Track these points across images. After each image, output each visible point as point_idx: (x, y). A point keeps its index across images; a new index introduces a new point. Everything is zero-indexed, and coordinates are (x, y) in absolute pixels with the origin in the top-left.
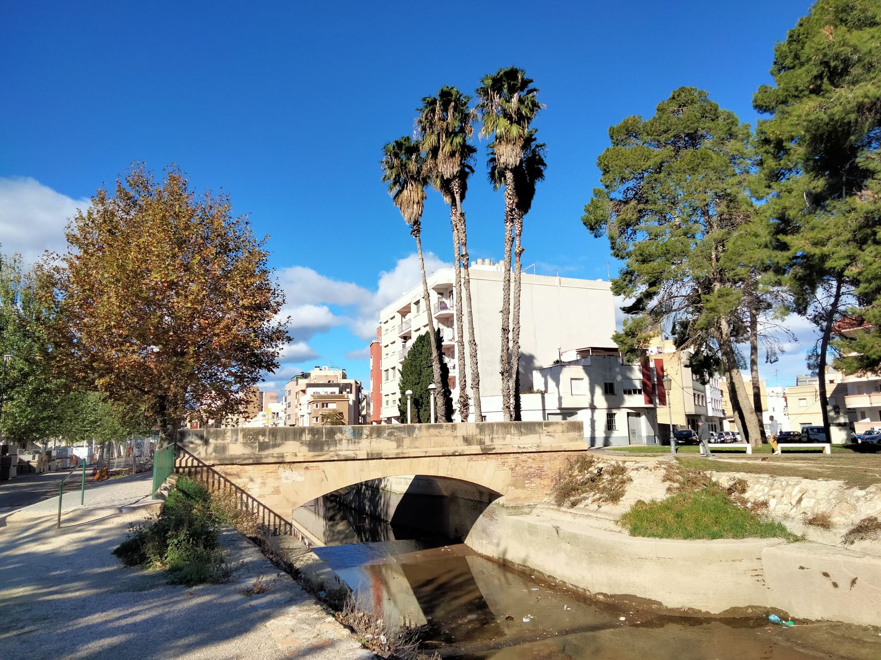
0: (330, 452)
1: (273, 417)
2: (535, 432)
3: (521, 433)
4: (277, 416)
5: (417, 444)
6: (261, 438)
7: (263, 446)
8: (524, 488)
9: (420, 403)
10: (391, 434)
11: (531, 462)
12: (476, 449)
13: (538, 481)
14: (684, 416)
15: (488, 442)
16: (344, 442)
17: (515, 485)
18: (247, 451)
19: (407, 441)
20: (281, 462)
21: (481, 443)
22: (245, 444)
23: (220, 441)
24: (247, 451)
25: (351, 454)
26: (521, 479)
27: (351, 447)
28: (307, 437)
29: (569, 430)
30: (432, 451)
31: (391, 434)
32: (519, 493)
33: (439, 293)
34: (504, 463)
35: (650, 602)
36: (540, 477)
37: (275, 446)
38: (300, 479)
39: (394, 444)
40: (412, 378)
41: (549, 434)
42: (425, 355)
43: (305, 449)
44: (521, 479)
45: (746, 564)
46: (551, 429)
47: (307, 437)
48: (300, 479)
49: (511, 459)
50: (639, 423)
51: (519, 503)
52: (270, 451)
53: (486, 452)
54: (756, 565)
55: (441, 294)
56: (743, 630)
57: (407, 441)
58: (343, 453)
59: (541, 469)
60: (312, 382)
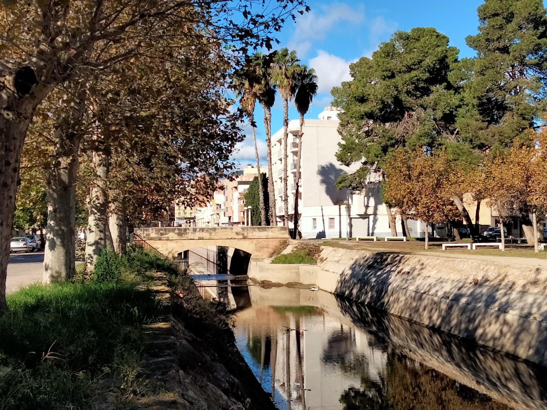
0: (185, 237)
1: (217, 208)
2: (266, 231)
3: (260, 231)
4: (220, 207)
5: (217, 234)
6: (161, 232)
7: (162, 234)
8: (260, 251)
9: (255, 212)
10: (207, 231)
11: (264, 243)
12: (241, 237)
13: (266, 249)
14: (490, 217)
15: (246, 234)
16: (190, 233)
17: (257, 250)
18: (157, 236)
19: (213, 233)
20: (168, 240)
21: (243, 234)
22: (156, 233)
23: (147, 232)
24: (157, 236)
25: (192, 238)
26: (260, 248)
27: (193, 235)
28: (177, 231)
29: (281, 230)
30: (223, 237)
31: (207, 231)
32: (259, 253)
33: (294, 135)
34: (252, 242)
35: (269, 281)
36: (267, 248)
37: (166, 234)
38: (175, 246)
39: (209, 234)
40: (249, 200)
41: (272, 232)
42: (256, 188)
43: (176, 235)
44: (260, 248)
45: (294, 270)
46: (273, 229)
47: (177, 231)
48: (175, 246)
49: (255, 241)
50: (416, 224)
51: (258, 257)
52: (164, 236)
53: (245, 238)
54: (297, 270)
55: (296, 136)
56: (292, 289)
57: (213, 233)
58: (189, 237)
59: (268, 245)
60: (244, 180)
